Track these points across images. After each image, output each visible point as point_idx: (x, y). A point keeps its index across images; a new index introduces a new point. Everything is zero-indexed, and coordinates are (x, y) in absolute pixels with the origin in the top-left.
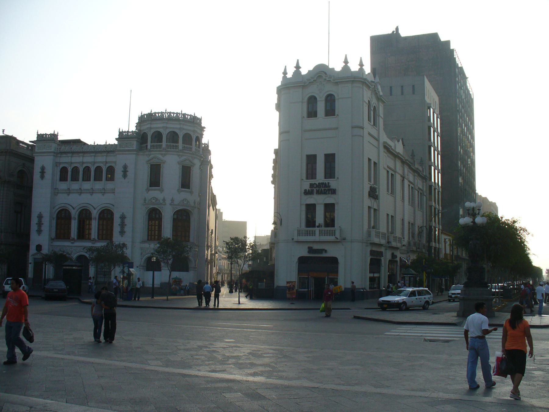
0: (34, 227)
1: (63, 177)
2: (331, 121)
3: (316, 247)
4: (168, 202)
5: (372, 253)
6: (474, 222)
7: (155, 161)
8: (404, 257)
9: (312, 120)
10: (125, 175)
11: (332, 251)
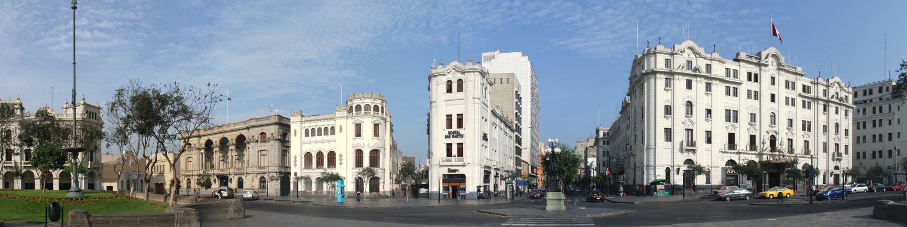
0: (292, 163)
1: (307, 135)
2: (461, 95)
3: (452, 168)
4: (366, 145)
5: (485, 171)
6: (553, 151)
7: (358, 122)
8: (503, 174)
9: (449, 94)
10: (341, 131)
11: (461, 171)
